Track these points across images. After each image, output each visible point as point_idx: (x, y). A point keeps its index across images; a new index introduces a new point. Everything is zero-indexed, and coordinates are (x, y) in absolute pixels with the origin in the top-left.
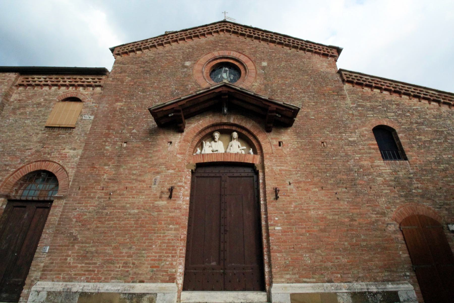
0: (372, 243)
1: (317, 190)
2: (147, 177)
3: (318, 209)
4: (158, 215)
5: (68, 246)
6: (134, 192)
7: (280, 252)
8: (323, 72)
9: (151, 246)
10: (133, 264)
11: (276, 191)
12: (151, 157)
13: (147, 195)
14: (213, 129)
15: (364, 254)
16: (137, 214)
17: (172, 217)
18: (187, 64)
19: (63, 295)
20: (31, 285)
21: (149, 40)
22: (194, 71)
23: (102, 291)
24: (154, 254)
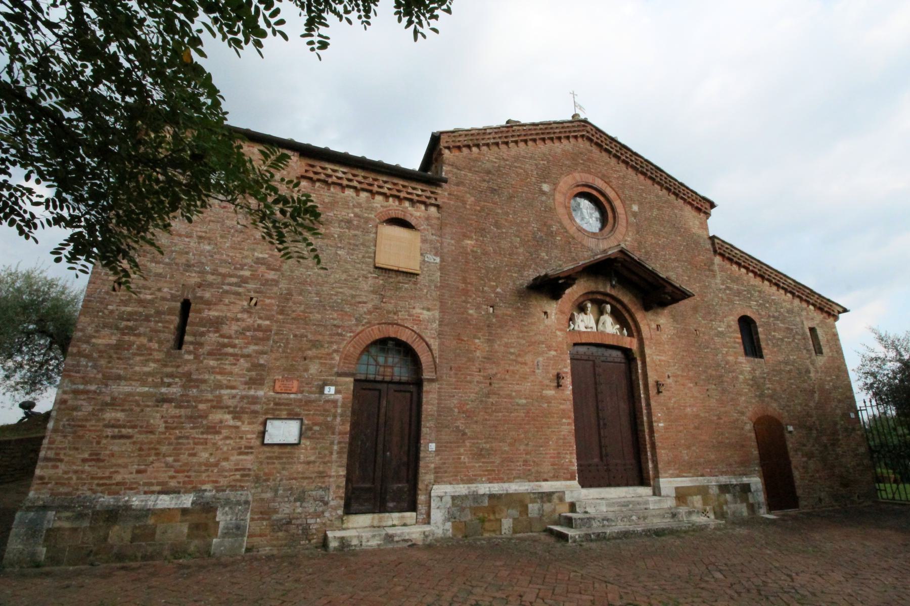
1: (691, 385)
7: (664, 448)
24: (552, 451)
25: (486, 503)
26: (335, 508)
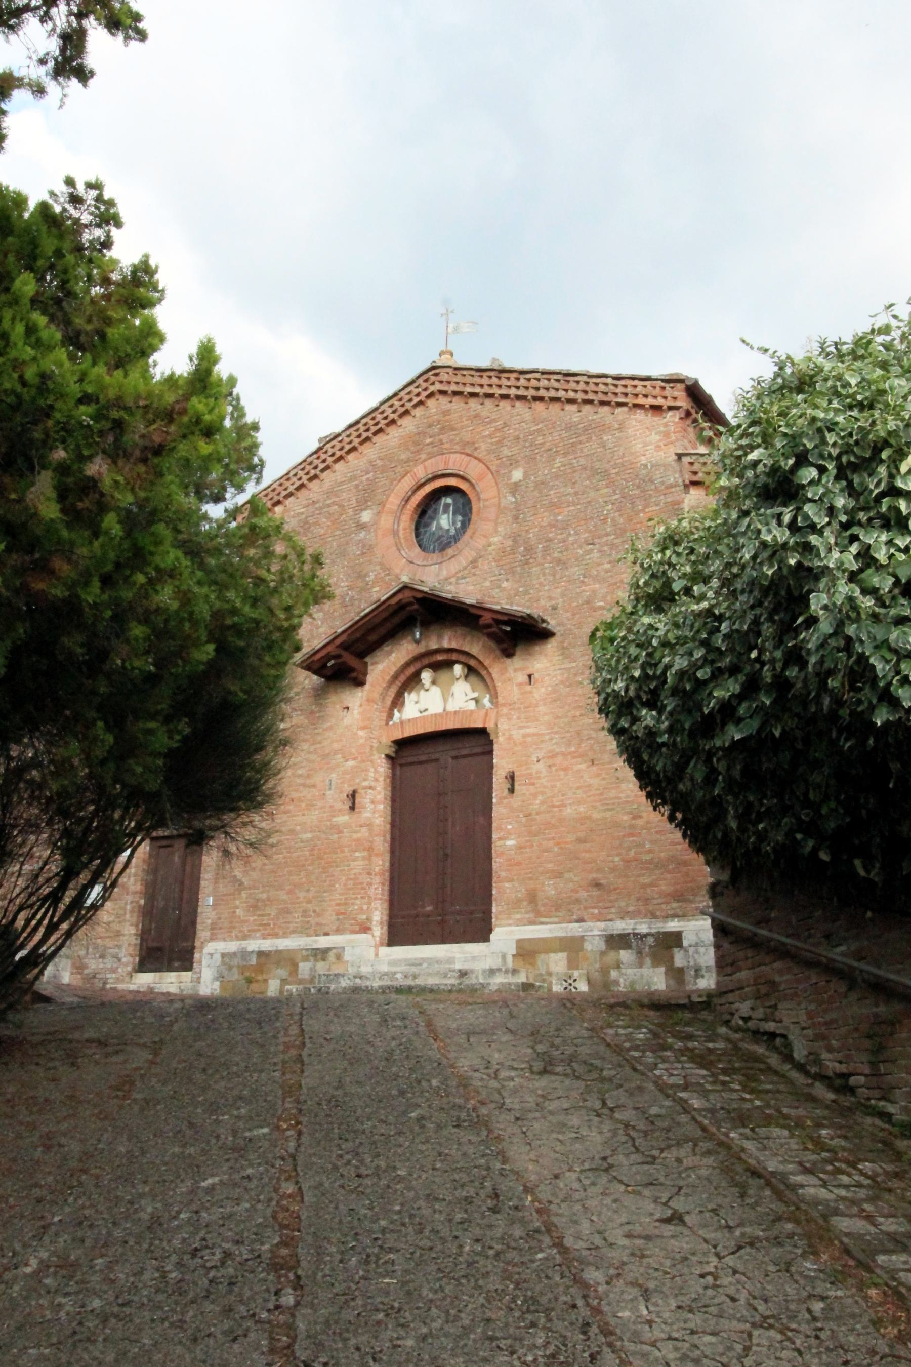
0: (662, 854)
1: (583, 766)
2: (317, 779)
3: (579, 803)
4: (339, 838)
5: (233, 894)
6: (303, 805)
7: (510, 880)
8: (646, 466)
9: (333, 886)
10: (314, 911)
11: (511, 778)
12: (320, 743)
13: (321, 808)
14: (418, 665)
15: (643, 875)
16: (312, 840)
17: (358, 840)
18: (366, 516)
19: (239, 956)
20: (202, 948)
21: (292, 474)
22: (380, 532)
23: (281, 948)
24: (338, 897)
25: (254, 961)
26: (127, 965)
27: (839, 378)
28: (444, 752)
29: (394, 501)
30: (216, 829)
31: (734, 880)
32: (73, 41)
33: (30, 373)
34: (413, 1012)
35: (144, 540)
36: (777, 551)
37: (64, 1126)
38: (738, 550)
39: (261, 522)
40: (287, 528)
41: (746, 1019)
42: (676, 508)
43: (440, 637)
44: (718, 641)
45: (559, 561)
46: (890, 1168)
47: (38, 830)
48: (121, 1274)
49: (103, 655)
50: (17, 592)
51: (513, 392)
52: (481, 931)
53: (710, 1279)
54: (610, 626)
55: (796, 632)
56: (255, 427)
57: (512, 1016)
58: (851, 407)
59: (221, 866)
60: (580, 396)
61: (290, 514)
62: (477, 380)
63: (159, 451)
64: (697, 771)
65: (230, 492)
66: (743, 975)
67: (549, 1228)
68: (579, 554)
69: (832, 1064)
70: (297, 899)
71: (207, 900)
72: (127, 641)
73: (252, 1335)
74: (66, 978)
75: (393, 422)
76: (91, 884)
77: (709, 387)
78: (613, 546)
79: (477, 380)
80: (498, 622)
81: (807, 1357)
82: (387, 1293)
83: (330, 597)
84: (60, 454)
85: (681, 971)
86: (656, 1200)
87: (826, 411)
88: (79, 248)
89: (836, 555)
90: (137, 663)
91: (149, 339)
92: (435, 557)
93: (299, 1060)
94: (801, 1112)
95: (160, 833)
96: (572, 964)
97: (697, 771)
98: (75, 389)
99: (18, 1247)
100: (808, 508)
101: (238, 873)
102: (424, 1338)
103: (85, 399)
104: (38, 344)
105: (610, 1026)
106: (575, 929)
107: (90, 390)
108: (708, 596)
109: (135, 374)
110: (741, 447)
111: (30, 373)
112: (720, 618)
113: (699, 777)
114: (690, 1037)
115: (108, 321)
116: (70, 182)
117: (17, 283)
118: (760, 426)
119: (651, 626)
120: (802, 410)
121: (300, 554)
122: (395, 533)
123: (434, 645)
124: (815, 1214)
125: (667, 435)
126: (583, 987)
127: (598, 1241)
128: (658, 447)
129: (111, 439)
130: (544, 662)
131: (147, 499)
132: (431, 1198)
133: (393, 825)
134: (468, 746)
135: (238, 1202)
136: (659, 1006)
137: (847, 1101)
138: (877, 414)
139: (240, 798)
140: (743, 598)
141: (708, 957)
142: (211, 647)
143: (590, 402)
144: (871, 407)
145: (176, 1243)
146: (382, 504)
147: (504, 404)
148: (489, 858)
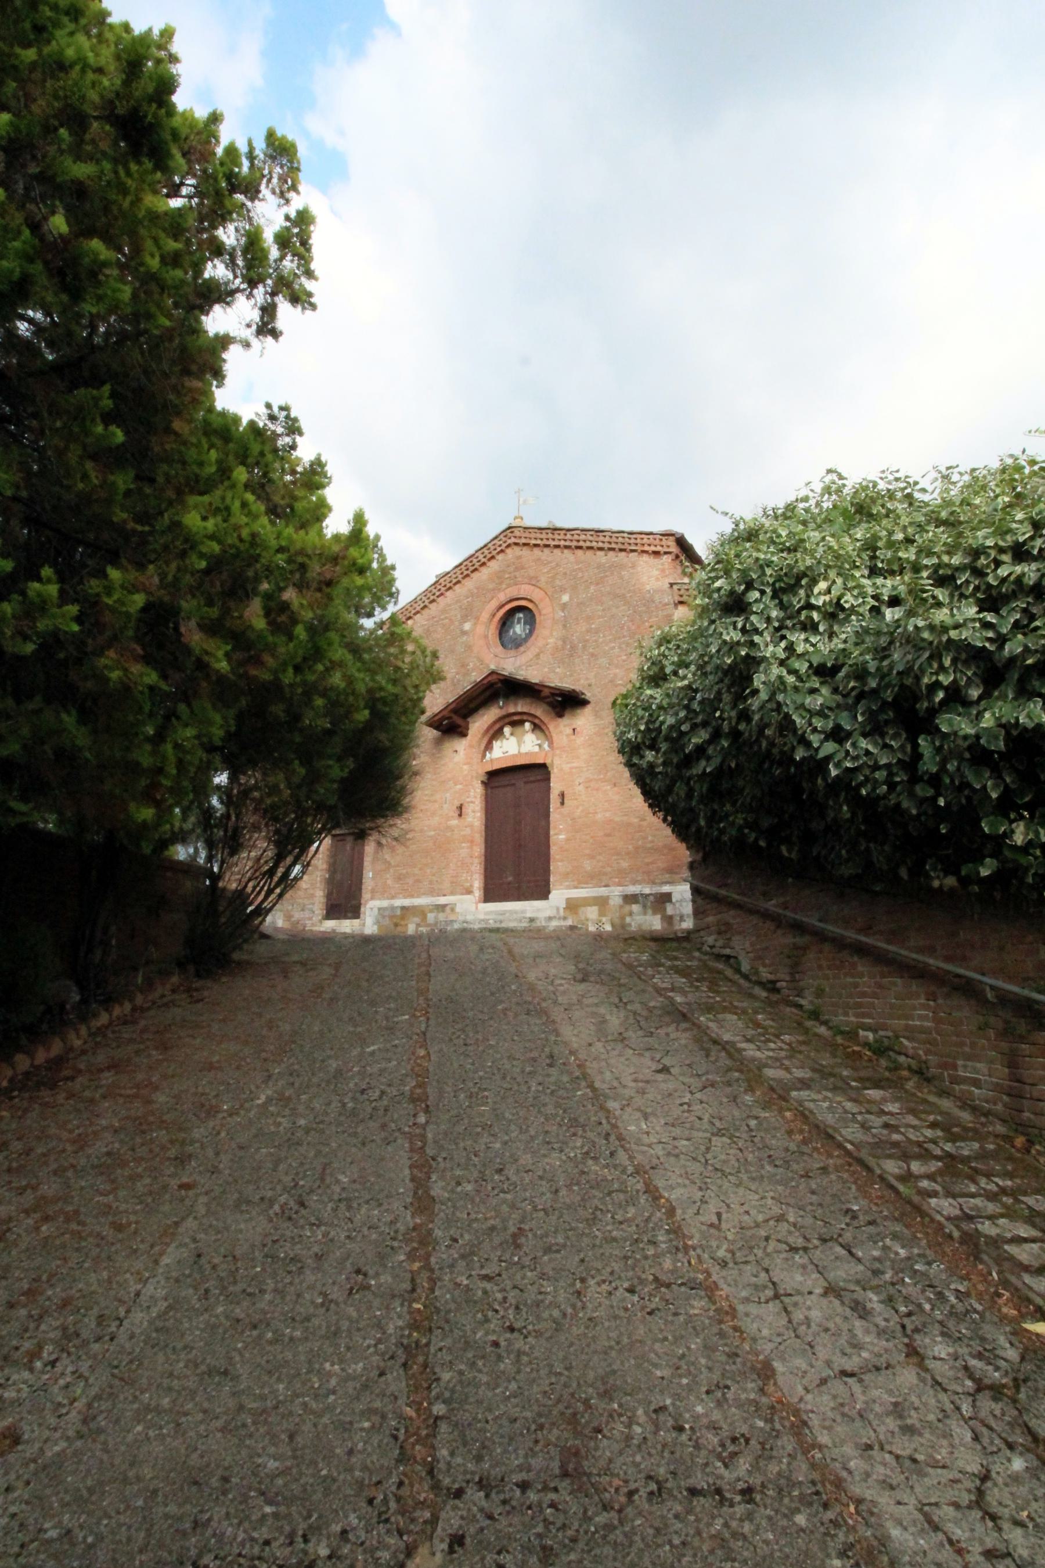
2: (437, 797)
11: (562, 795)
18: (467, 626)
25: (399, 912)
27: (775, 531)
28: (519, 780)
29: (485, 616)
30: (371, 829)
31: (704, 859)
32: (268, 311)
33: (245, 533)
34: (499, 944)
35: (323, 644)
36: (733, 646)
37: (280, 1015)
38: (708, 646)
39: (398, 630)
40: (414, 634)
41: (711, 947)
42: (669, 619)
43: (516, 705)
44: (695, 706)
45: (593, 655)
46: (801, 1038)
47: (260, 830)
48: (316, 1105)
49: (297, 718)
50: (240, 676)
51: (562, 543)
52: (543, 893)
53: (686, 1107)
54: (625, 697)
55: (745, 699)
56: (393, 568)
57: (563, 946)
58: (782, 551)
59: (376, 852)
60: (606, 546)
61: (417, 626)
62: (539, 536)
63: (329, 583)
64: (680, 789)
65: (378, 610)
66: (710, 919)
67: (585, 1076)
68: (608, 648)
69: (765, 974)
70: (424, 872)
71: (368, 875)
72: (313, 708)
73: (399, 1141)
74: (280, 923)
75: (484, 564)
76: (294, 864)
77: (690, 539)
78: (628, 645)
79: (539, 536)
80: (553, 695)
81: (746, 1153)
82: (483, 1116)
83: (443, 679)
84: (265, 586)
85: (671, 917)
86: (652, 1059)
87: (766, 553)
88: (276, 450)
89: (771, 648)
90: (319, 723)
91: (321, 510)
92: (513, 652)
93: (428, 974)
94: (745, 1004)
95: (337, 832)
96: (602, 913)
97: (680, 789)
98: (274, 544)
99: (253, 1088)
100: (754, 618)
101: (387, 857)
102: (506, 1143)
103: (281, 550)
104: (249, 514)
105: (624, 952)
106: (603, 891)
107: (283, 544)
108: (688, 676)
109: (313, 533)
110: (710, 578)
111: (245, 533)
112: (696, 691)
113: (682, 794)
114: (676, 958)
115: (295, 498)
116: (268, 406)
117: (235, 474)
118: (723, 565)
119: (651, 697)
120: (750, 553)
121: (423, 652)
122: (486, 637)
123: (512, 710)
124: (751, 1066)
125: (663, 571)
126: (608, 928)
127: (615, 1084)
128: (657, 579)
129: (297, 576)
130: (583, 720)
131: (323, 616)
132: (511, 1058)
133: (487, 827)
134: (533, 776)
135: (390, 1060)
136: (657, 939)
137: (775, 997)
138: (799, 555)
139: (388, 809)
140: (711, 677)
141: (688, 909)
142: (367, 712)
143: (613, 549)
144: (795, 551)
145: (351, 1085)
146: (477, 618)
147: (557, 551)
148: (548, 847)
